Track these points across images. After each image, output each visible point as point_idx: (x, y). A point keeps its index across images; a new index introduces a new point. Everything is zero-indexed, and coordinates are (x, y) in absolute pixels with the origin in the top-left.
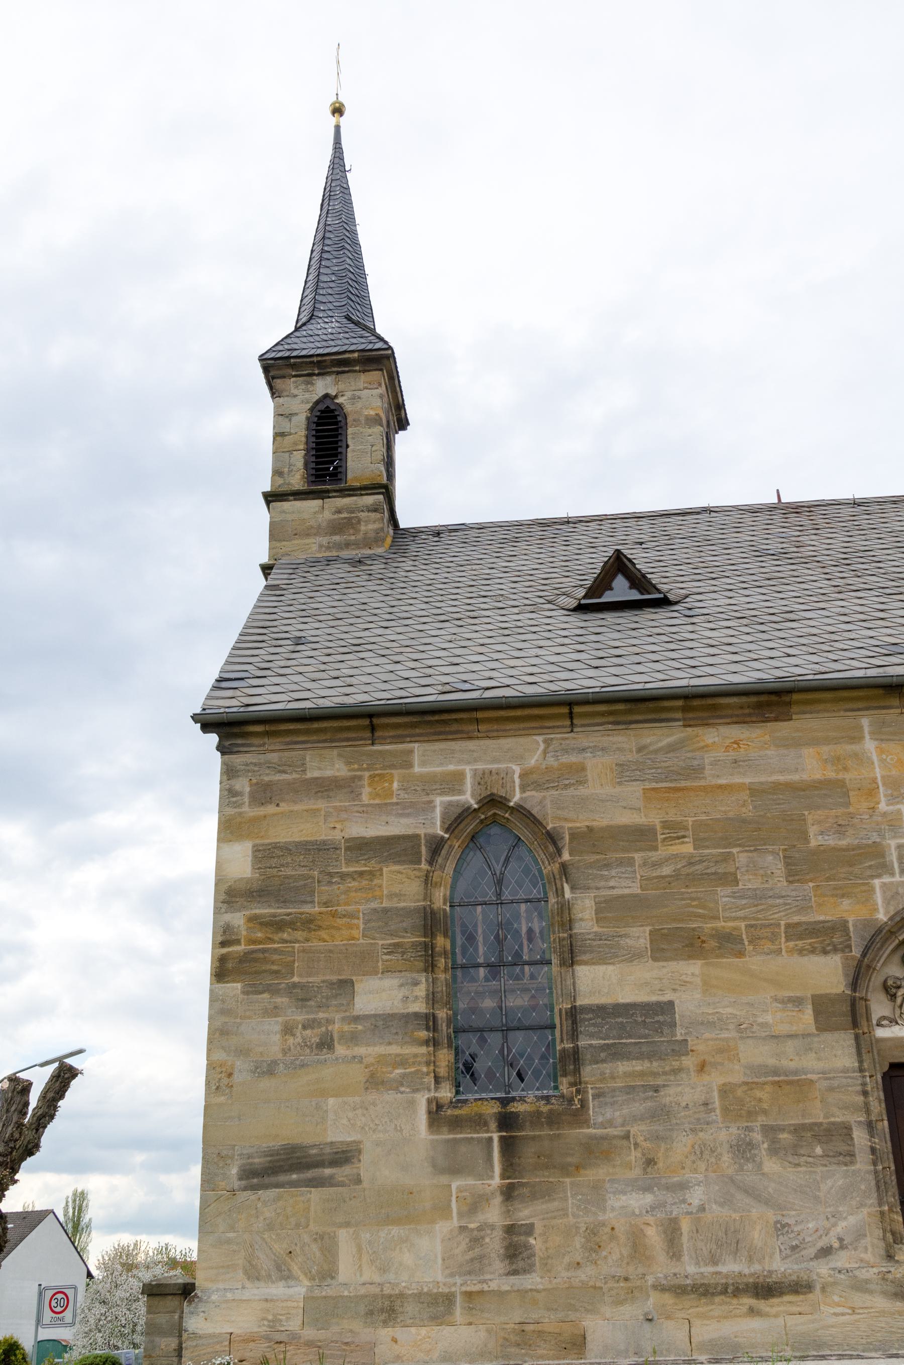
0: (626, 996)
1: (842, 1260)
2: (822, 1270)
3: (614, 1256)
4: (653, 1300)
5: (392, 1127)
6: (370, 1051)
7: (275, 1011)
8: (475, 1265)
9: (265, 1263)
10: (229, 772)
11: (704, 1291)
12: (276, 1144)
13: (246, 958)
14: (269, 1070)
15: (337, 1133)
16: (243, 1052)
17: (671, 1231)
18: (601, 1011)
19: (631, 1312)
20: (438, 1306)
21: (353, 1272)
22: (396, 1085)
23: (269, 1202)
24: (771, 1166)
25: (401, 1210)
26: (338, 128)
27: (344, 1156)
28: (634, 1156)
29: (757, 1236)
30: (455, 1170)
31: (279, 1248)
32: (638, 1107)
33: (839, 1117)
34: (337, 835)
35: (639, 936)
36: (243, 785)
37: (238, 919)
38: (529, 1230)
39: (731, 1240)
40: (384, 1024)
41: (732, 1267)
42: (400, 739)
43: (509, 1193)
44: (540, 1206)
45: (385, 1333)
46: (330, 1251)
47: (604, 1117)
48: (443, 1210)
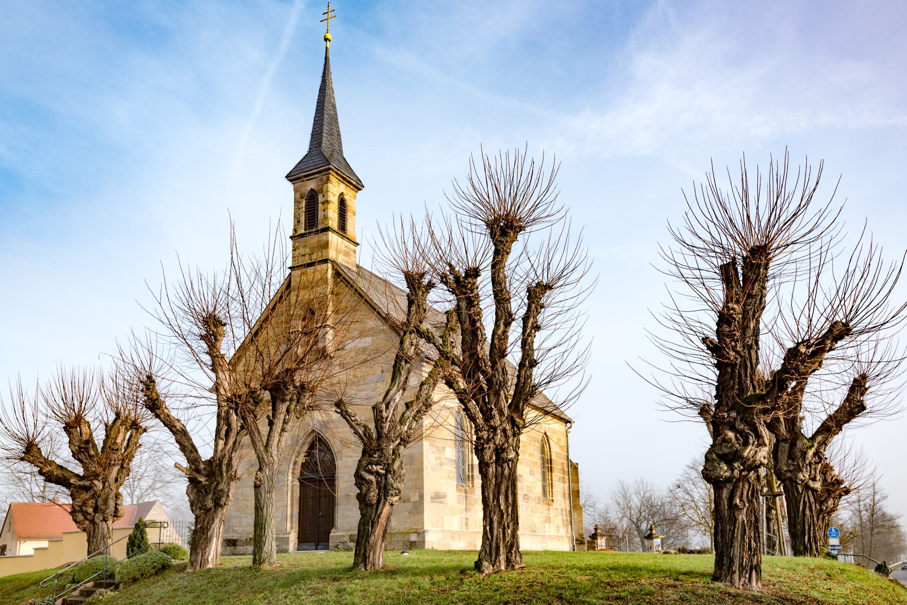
7: (434, 452)
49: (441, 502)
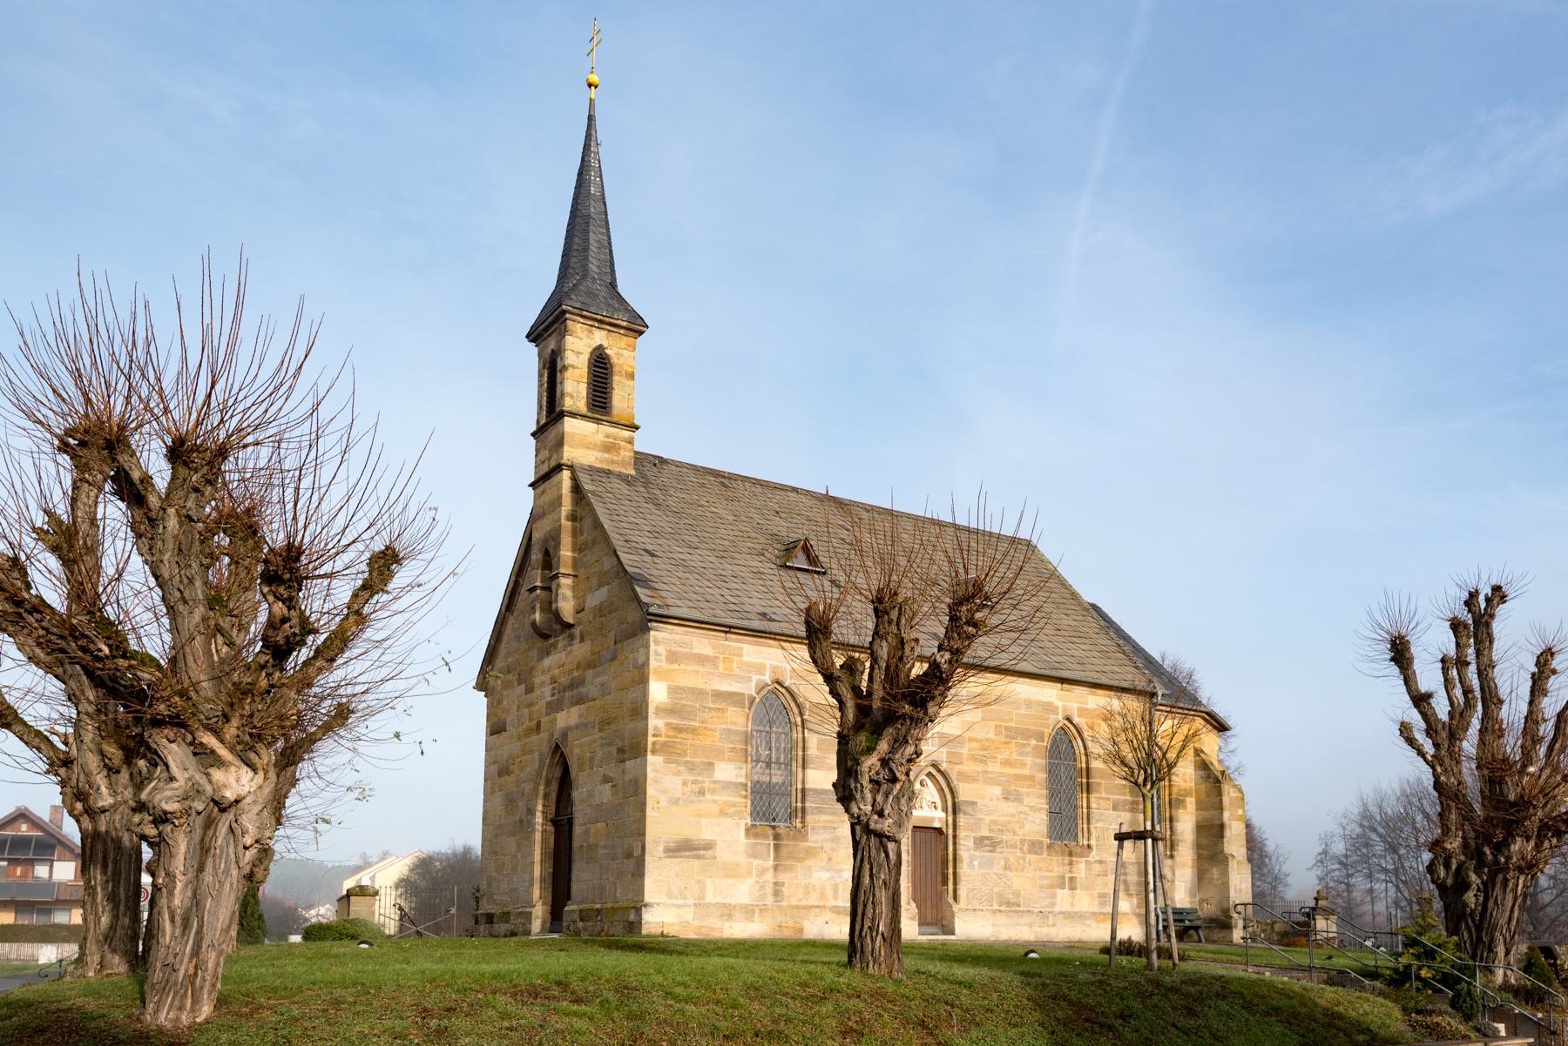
6: (722, 798)
7: (678, 773)
12: (680, 838)
13: (665, 744)
14: (675, 802)
15: (707, 835)
16: (664, 792)
18: (815, 791)
22: (732, 816)
25: (732, 872)
27: (709, 846)
28: (824, 856)
30: (755, 856)
32: (827, 836)
38: (783, 884)
40: (727, 785)
43: (776, 868)
44: (787, 874)
45: (727, 924)
46: (703, 889)
48: (749, 874)
49: (698, 857)
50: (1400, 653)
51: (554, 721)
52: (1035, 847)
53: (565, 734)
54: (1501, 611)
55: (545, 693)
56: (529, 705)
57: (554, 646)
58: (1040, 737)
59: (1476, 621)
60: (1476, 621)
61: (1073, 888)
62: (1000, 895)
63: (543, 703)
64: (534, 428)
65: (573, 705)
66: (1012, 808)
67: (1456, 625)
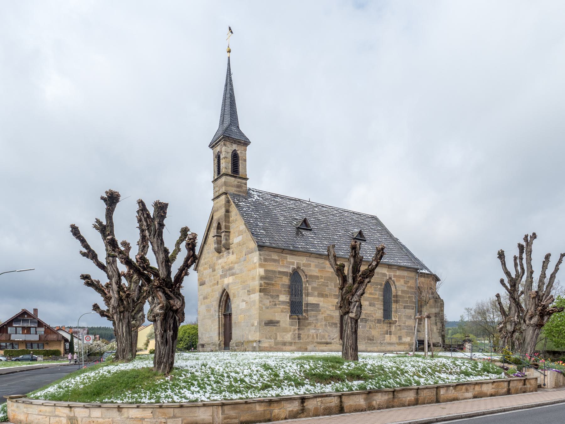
0: (314, 302)
1: (335, 340)
2: (333, 341)
3: (311, 338)
4: (315, 344)
5: (284, 318)
6: (282, 307)
7: (268, 299)
8: (294, 339)
9: (268, 337)
10: (260, 255)
11: (321, 343)
13: (264, 289)
14: (267, 308)
15: (277, 319)
16: (264, 305)
17: (317, 335)
18: (310, 304)
19: (313, 346)
20: (291, 344)
21: (279, 339)
23: (268, 328)
24: (329, 328)
25: (285, 330)
26: (229, 57)
27: (278, 322)
29: (326, 337)
30: (292, 325)
31: (270, 335)
32: (314, 318)
33: (336, 322)
34: (276, 270)
35: (316, 293)
36: (262, 257)
37: (262, 282)
39: (323, 337)
40: (283, 303)
41: (323, 340)
42: (286, 254)
43: (299, 329)
45: (284, 347)
46: (276, 335)
47: (311, 319)
48: (290, 331)
49: (275, 326)
50: (501, 255)
51: (223, 281)
52: (379, 321)
53: (228, 285)
54: (535, 241)
55: (220, 272)
56: (214, 276)
57: (223, 256)
58: (381, 285)
59: (525, 248)
60: (525, 248)
61: (390, 334)
62: (368, 337)
63: (219, 275)
64: (213, 180)
65: (230, 276)
66: (372, 308)
67: (521, 247)
